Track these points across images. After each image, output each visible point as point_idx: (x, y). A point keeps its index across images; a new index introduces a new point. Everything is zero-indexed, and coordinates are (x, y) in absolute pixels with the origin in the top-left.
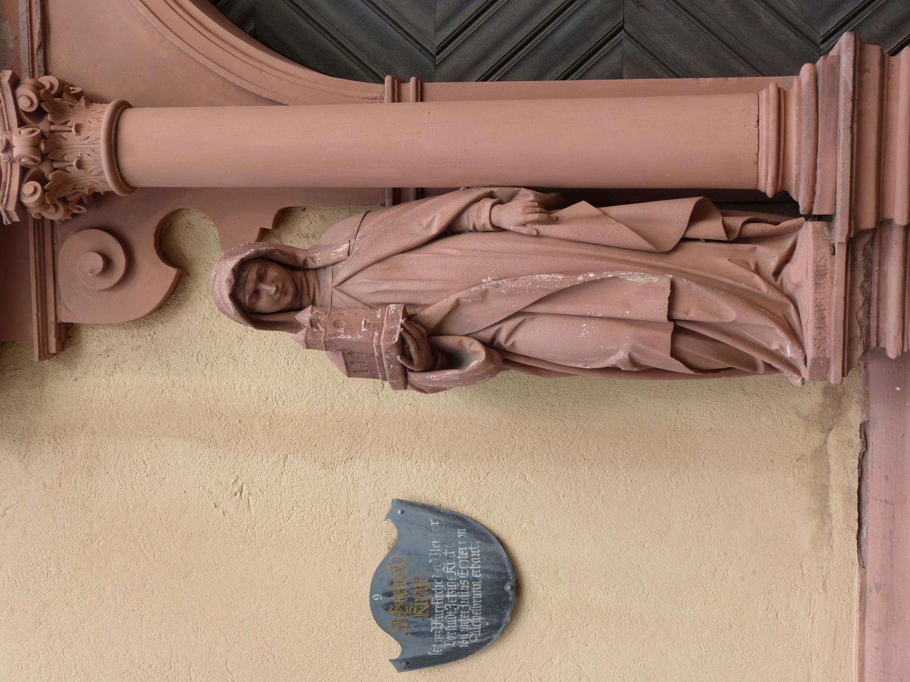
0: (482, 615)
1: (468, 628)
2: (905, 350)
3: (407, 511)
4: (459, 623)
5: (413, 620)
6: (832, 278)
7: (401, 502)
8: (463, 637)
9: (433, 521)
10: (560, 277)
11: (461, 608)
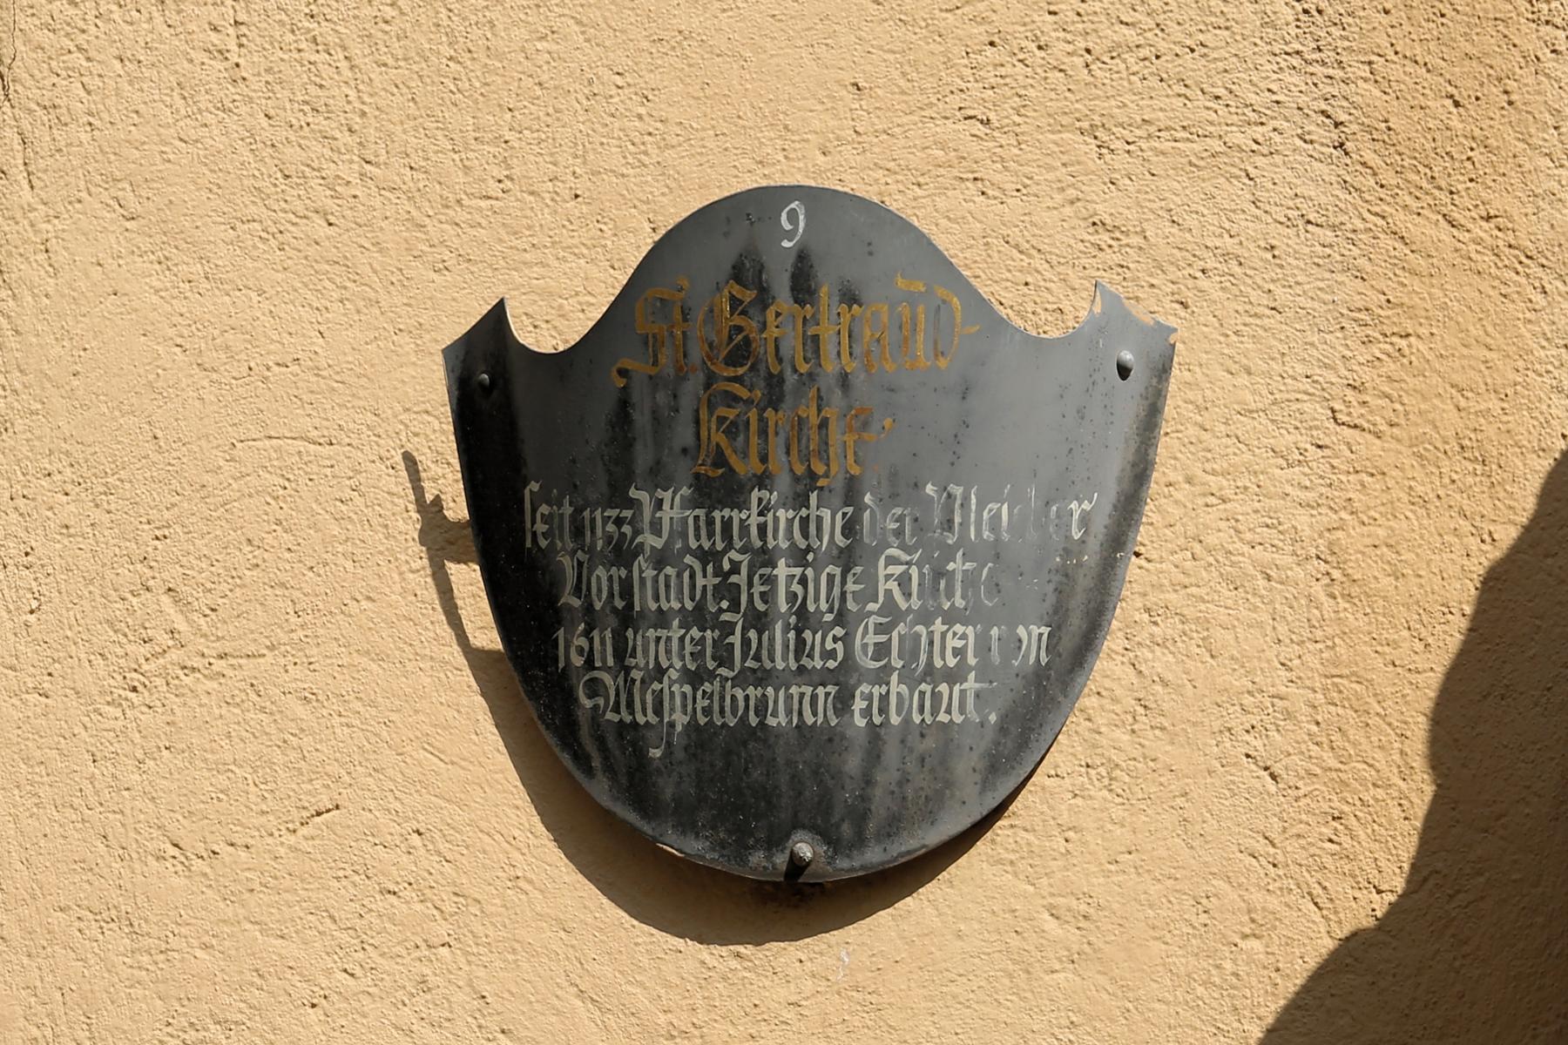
0: (692, 726)
1: (640, 663)
3: (1145, 377)
4: (662, 620)
5: (686, 403)
7: (1163, 371)
8: (604, 642)
9: (1086, 510)
11: (728, 629)
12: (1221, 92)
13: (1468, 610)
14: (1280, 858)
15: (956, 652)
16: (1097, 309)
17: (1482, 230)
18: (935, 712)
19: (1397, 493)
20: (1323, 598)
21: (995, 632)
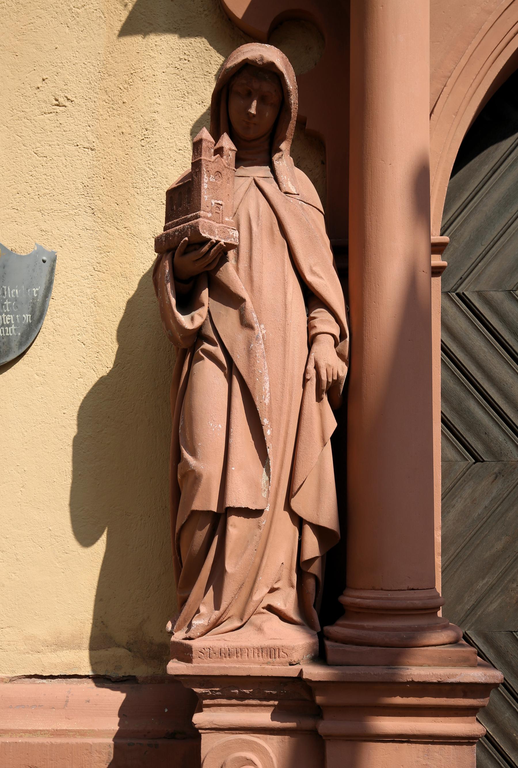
2: (200, 731)
3: (51, 263)
6: (267, 663)
7: (54, 261)
9: (37, 290)
10: (267, 401)
12: (67, 203)
13: (124, 308)
14: (86, 361)
15: (9, 321)
16: (36, 249)
17: (124, 230)
18: (5, 333)
19: (108, 285)
20: (93, 307)
21: (17, 316)
